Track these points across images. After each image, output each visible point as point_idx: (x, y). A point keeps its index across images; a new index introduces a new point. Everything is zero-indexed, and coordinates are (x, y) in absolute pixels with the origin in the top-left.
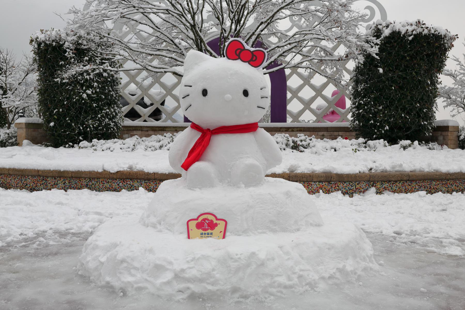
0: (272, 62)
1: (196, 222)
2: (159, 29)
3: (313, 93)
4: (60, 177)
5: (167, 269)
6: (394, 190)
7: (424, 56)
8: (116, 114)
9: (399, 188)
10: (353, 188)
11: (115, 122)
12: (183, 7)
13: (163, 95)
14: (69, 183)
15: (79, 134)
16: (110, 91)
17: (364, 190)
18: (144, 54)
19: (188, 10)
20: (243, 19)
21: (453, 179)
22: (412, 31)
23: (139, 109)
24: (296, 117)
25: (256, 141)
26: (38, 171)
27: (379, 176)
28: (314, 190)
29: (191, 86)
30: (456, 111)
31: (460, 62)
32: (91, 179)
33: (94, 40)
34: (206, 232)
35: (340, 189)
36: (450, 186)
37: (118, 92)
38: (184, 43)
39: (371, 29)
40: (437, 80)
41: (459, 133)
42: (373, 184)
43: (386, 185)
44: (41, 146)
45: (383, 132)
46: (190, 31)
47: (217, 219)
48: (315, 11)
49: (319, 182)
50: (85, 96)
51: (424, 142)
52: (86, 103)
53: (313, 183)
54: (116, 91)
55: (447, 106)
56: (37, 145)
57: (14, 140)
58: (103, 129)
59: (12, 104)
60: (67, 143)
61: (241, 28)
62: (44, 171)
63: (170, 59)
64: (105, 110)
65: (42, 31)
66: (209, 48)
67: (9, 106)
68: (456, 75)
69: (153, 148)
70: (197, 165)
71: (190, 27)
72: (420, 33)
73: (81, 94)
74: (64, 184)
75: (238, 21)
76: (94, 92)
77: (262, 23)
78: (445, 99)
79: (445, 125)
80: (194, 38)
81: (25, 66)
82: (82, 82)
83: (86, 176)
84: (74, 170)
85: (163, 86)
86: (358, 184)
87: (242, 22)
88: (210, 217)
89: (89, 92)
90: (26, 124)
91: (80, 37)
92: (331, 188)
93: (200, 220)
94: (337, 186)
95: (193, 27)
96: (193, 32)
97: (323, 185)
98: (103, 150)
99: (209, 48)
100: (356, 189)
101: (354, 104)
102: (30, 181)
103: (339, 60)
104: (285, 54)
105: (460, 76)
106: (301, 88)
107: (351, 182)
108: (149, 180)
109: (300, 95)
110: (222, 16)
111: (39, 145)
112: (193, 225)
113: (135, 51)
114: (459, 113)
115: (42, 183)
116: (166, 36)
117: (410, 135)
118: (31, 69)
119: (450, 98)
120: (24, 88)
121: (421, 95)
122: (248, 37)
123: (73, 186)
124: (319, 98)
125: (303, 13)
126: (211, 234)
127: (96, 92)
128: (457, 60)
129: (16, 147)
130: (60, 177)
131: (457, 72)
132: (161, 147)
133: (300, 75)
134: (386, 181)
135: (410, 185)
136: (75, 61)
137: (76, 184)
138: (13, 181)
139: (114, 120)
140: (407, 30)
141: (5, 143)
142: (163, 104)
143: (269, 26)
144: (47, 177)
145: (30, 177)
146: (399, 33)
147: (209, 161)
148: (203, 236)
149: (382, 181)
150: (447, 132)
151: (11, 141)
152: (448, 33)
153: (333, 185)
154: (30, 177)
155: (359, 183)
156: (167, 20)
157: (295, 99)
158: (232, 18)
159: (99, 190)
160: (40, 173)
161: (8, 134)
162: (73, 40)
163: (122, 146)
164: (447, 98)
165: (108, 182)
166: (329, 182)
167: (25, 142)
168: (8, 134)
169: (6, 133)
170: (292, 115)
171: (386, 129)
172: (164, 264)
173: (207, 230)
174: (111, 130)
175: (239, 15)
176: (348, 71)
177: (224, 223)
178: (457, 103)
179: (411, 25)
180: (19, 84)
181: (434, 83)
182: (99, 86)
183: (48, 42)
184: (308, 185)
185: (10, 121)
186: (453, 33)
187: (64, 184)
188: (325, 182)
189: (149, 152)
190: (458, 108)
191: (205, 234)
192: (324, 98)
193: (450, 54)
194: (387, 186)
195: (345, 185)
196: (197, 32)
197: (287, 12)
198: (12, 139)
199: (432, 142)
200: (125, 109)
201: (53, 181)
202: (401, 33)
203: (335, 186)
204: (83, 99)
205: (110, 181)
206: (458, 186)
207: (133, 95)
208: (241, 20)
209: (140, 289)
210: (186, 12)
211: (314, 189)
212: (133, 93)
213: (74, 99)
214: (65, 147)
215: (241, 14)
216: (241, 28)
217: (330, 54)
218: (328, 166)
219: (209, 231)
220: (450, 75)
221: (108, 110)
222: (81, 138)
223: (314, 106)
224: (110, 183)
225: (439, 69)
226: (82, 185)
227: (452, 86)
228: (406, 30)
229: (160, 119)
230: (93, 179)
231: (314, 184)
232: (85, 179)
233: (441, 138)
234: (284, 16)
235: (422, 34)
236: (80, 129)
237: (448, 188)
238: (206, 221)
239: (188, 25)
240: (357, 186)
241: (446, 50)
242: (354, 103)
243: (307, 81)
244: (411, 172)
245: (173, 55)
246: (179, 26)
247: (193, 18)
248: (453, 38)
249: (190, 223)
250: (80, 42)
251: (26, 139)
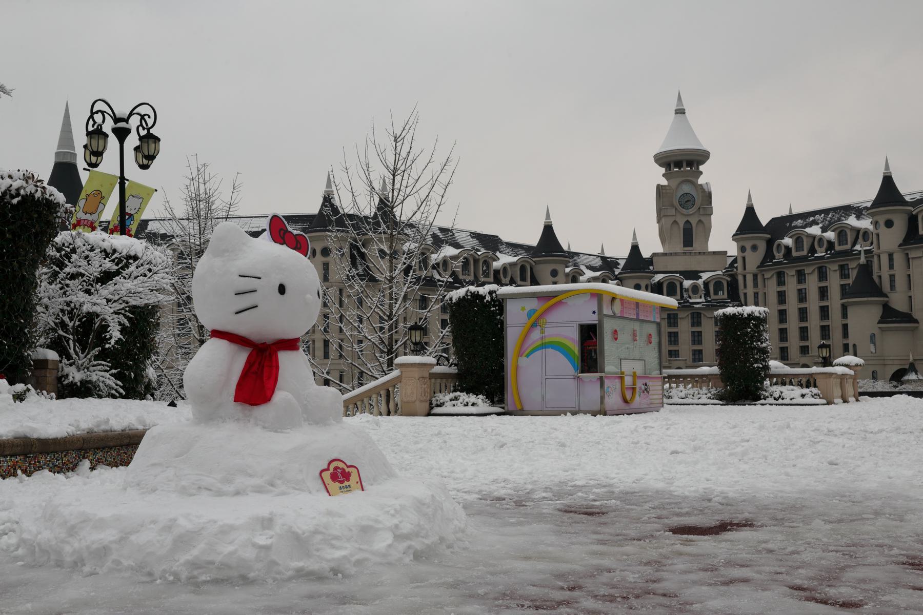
5: (377, 530)
9: (114, 459)
10: (59, 463)
17: (73, 466)
27: (95, 440)
28: (4, 472)
29: (260, 278)
34: (344, 485)
35: (41, 467)
41: (58, 372)
43: (100, 454)
49: (11, 457)
72: (31, 193)
88: (341, 465)
92: (28, 466)
97: (17, 462)
100: (63, 464)
107: (57, 454)
140: (11, 185)
148: (343, 490)
150: (43, 371)
153: (31, 460)
155: (67, 453)
166: (26, 455)
172: (371, 523)
188: (19, 456)
194: (101, 455)
195: (48, 459)
203: (35, 462)
209: (359, 563)
211: (3, 470)
218: (22, 426)
219: (346, 483)
228: (8, 185)
231: (3, 461)
235: (34, 196)
238: (338, 470)
240: (65, 460)
244: (122, 431)
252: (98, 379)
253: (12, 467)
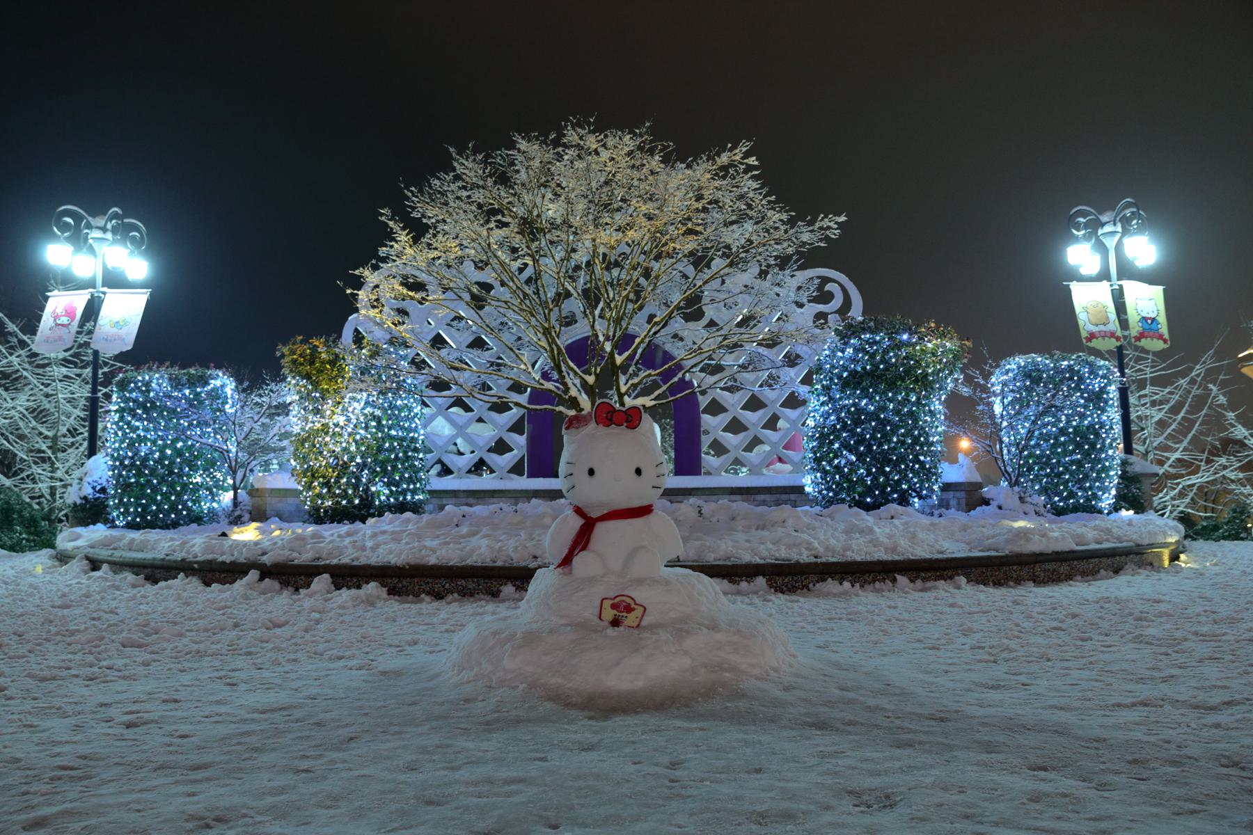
88: (629, 600)
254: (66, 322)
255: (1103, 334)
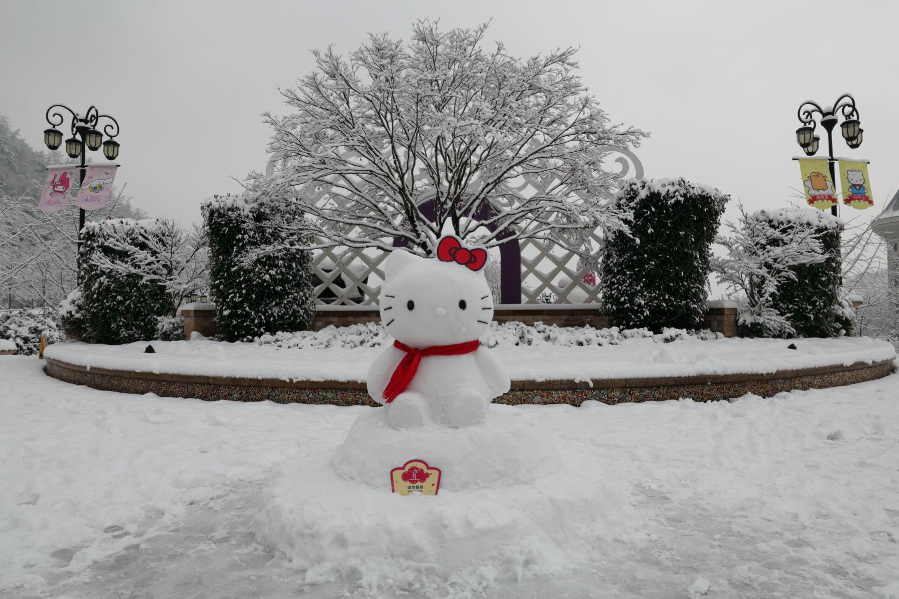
0: (501, 232)
1: (402, 471)
2: (360, 192)
3: (554, 266)
4: (235, 386)
6: (656, 398)
7: (690, 222)
8: (307, 298)
11: (305, 309)
12: (389, 165)
13: (366, 270)
14: (247, 393)
15: (261, 325)
16: (298, 270)
18: (341, 224)
19: (395, 169)
20: (464, 179)
21: (730, 383)
22: (675, 192)
23: (335, 288)
24: (532, 298)
25: (477, 363)
26: (208, 378)
30: (732, 288)
31: (735, 228)
32: (274, 388)
33: (279, 208)
34: (415, 485)
36: (727, 391)
37: (309, 271)
38: (390, 209)
39: (624, 190)
40: (708, 252)
42: (630, 392)
43: (647, 392)
44: (213, 340)
45: (642, 318)
46: (398, 194)
47: (428, 468)
48: (555, 169)
50: (267, 277)
51: (693, 330)
52: (268, 286)
53: (554, 392)
54: (307, 269)
55: (721, 282)
56: (209, 338)
57: (180, 331)
58: (290, 318)
59: (178, 287)
60: (245, 336)
61: (461, 191)
62: (215, 378)
63: (373, 229)
64: (293, 294)
65: (216, 197)
66: (421, 216)
67: (174, 290)
68: (731, 243)
69: (352, 344)
70: (401, 398)
71: (398, 190)
73: (263, 274)
74: (240, 394)
75: (459, 182)
76: (279, 272)
77: (488, 184)
78: (719, 274)
79: (720, 306)
80: (403, 203)
81: (194, 240)
82: (265, 259)
83: (267, 385)
84: (252, 377)
85: (365, 258)
86: (611, 392)
87: (463, 183)
88: (420, 466)
89: (273, 272)
90: (195, 311)
91: (262, 204)
93: (406, 469)
94: (585, 395)
95: (402, 191)
96: (402, 196)
98: (289, 347)
99: (421, 216)
100: (609, 398)
101: (605, 282)
102: (198, 389)
103: (585, 227)
104: (517, 221)
105: (736, 245)
106: (538, 260)
108: (346, 390)
109: (537, 268)
110: (438, 175)
111: (211, 337)
112: (398, 475)
113: (330, 220)
114: (737, 291)
115: (212, 393)
116: (368, 200)
117: (676, 321)
118: (202, 242)
119: (725, 273)
120: (194, 266)
121: (689, 271)
122: (471, 200)
123: (251, 397)
124: (562, 273)
125: (540, 170)
126: (422, 487)
127: (281, 271)
128: (731, 226)
129: (182, 342)
130: (235, 386)
131: (732, 240)
132: (362, 343)
133: (537, 245)
134: (646, 388)
135: (676, 392)
136: (255, 234)
137: (255, 394)
138: (177, 390)
139: (303, 306)
140: (669, 190)
141: (170, 335)
142: (365, 281)
143: (497, 186)
144: (220, 386)
145: (198, 385)
146: (659, 194)
147: (418, 391)
149: (640, 387)
151: (176, 332)
152: (718, 193)
154: (198, 385)
155: (613, 390)
156: (370, 180)
157: (531, 274)
158: (450, 180)
159: (284, 402)
160: (211, 381)
161: (173, 324)
162: (253, 208)
163: (314, 342)
164: (721, 273)
165: (295, 393)
166: (574, 390)
167: (194, 334)
168: (173, 324)
169: (170, 323)
170: (527, 294)
171: (645, 314)
173: (416, 482)
174: (300, 319)
175: (460, 175)
176: (596, 238)
177: (437, 473)
178: (735, 278)
179: (673, 184)
180: (187, 261)
181: (704, 257)
182: (284, 265)
183: (221, 211)
184: (548, 395)
185: (176, 308)
186: (724, 192)
187: (240, 394)
189: (347, 350)
190: (735, 284)
191: (413, 487)
192: (568, 272)
193: (722, 218)
195: (595, 393)
196: (406, 196)
197: (519, 169)
198: (177, 330)
199: (704, 329)
200: (318, 289)
201: (226, 391)
202: (661, 194)
204: (265, 281)
205: (297, 391)
206: (736, 391)
207: (328, 271)
208: (462, 180)
210: (392, 170)
212: (329, 268)
213: (254, 281)
214: (242, 341)
215: (462, 173)
216: (461, 191)
217: (574, 221)
219: (419, 484)
220: (724, 244)
221: (296, 294)
222: (262, 330)
223: (555, 282)
224: (297, 394)
225: (710, 235)
226: (262, 395)
227: (728, 258)
229: (362, 301)
230: (276, 388)
232: (266, 388)
233: (715, 324)
234: (516, 173)
236: (261, 319)
237: (724, 394)
238: (415, 470)
239: (396, 188)
241: (717, 214)
242: (605, 281)
243: (545, 252)
245: (378, 224)
246: (384, 188)
247: (402, 178)
248: (725, 200)
249: (394, 473)
250: (262, 210)
251: (195, 330)
252: (764, 322)
253: (562, 398)
254: (62, 190)
255: (822, 197)
